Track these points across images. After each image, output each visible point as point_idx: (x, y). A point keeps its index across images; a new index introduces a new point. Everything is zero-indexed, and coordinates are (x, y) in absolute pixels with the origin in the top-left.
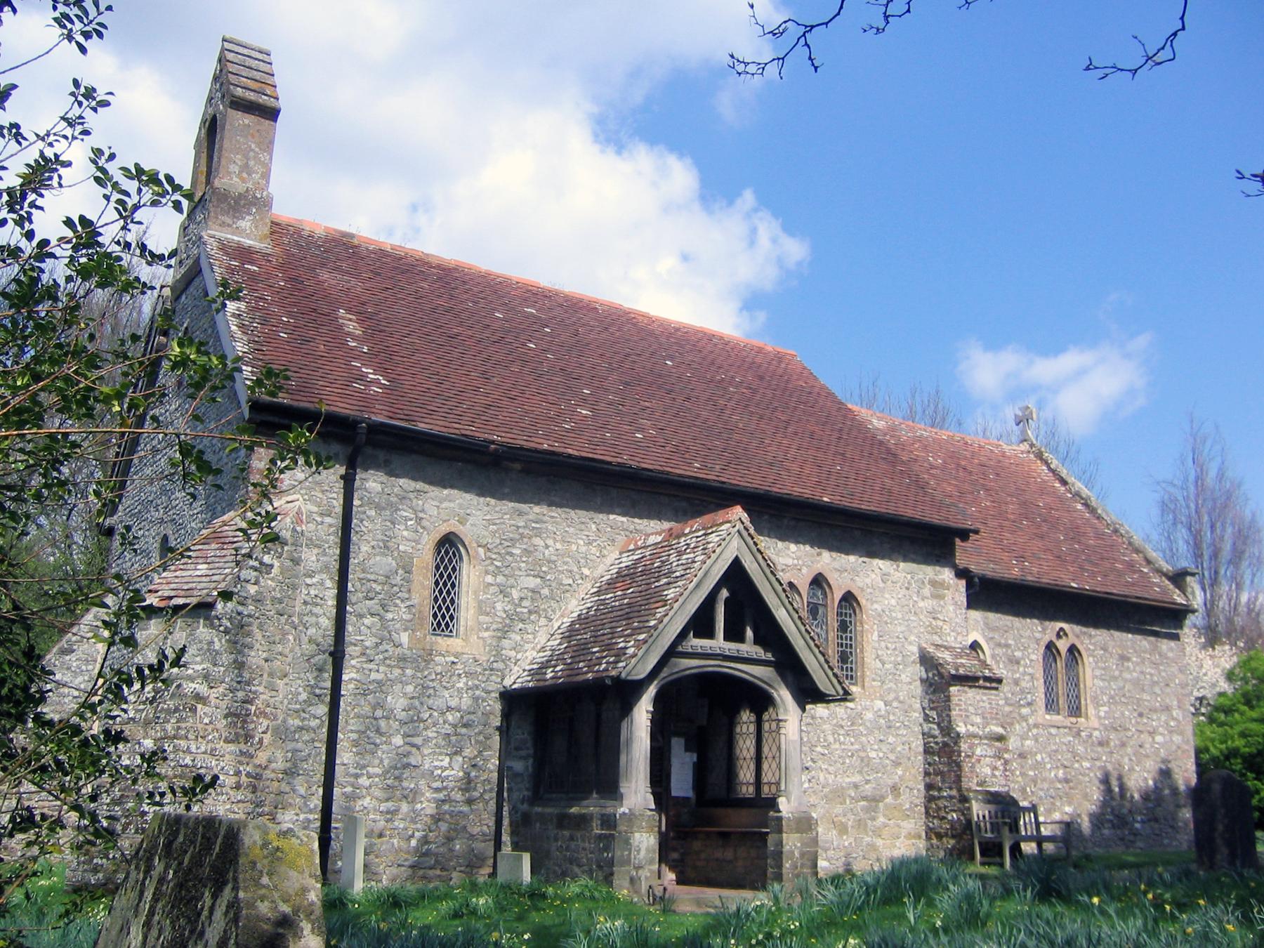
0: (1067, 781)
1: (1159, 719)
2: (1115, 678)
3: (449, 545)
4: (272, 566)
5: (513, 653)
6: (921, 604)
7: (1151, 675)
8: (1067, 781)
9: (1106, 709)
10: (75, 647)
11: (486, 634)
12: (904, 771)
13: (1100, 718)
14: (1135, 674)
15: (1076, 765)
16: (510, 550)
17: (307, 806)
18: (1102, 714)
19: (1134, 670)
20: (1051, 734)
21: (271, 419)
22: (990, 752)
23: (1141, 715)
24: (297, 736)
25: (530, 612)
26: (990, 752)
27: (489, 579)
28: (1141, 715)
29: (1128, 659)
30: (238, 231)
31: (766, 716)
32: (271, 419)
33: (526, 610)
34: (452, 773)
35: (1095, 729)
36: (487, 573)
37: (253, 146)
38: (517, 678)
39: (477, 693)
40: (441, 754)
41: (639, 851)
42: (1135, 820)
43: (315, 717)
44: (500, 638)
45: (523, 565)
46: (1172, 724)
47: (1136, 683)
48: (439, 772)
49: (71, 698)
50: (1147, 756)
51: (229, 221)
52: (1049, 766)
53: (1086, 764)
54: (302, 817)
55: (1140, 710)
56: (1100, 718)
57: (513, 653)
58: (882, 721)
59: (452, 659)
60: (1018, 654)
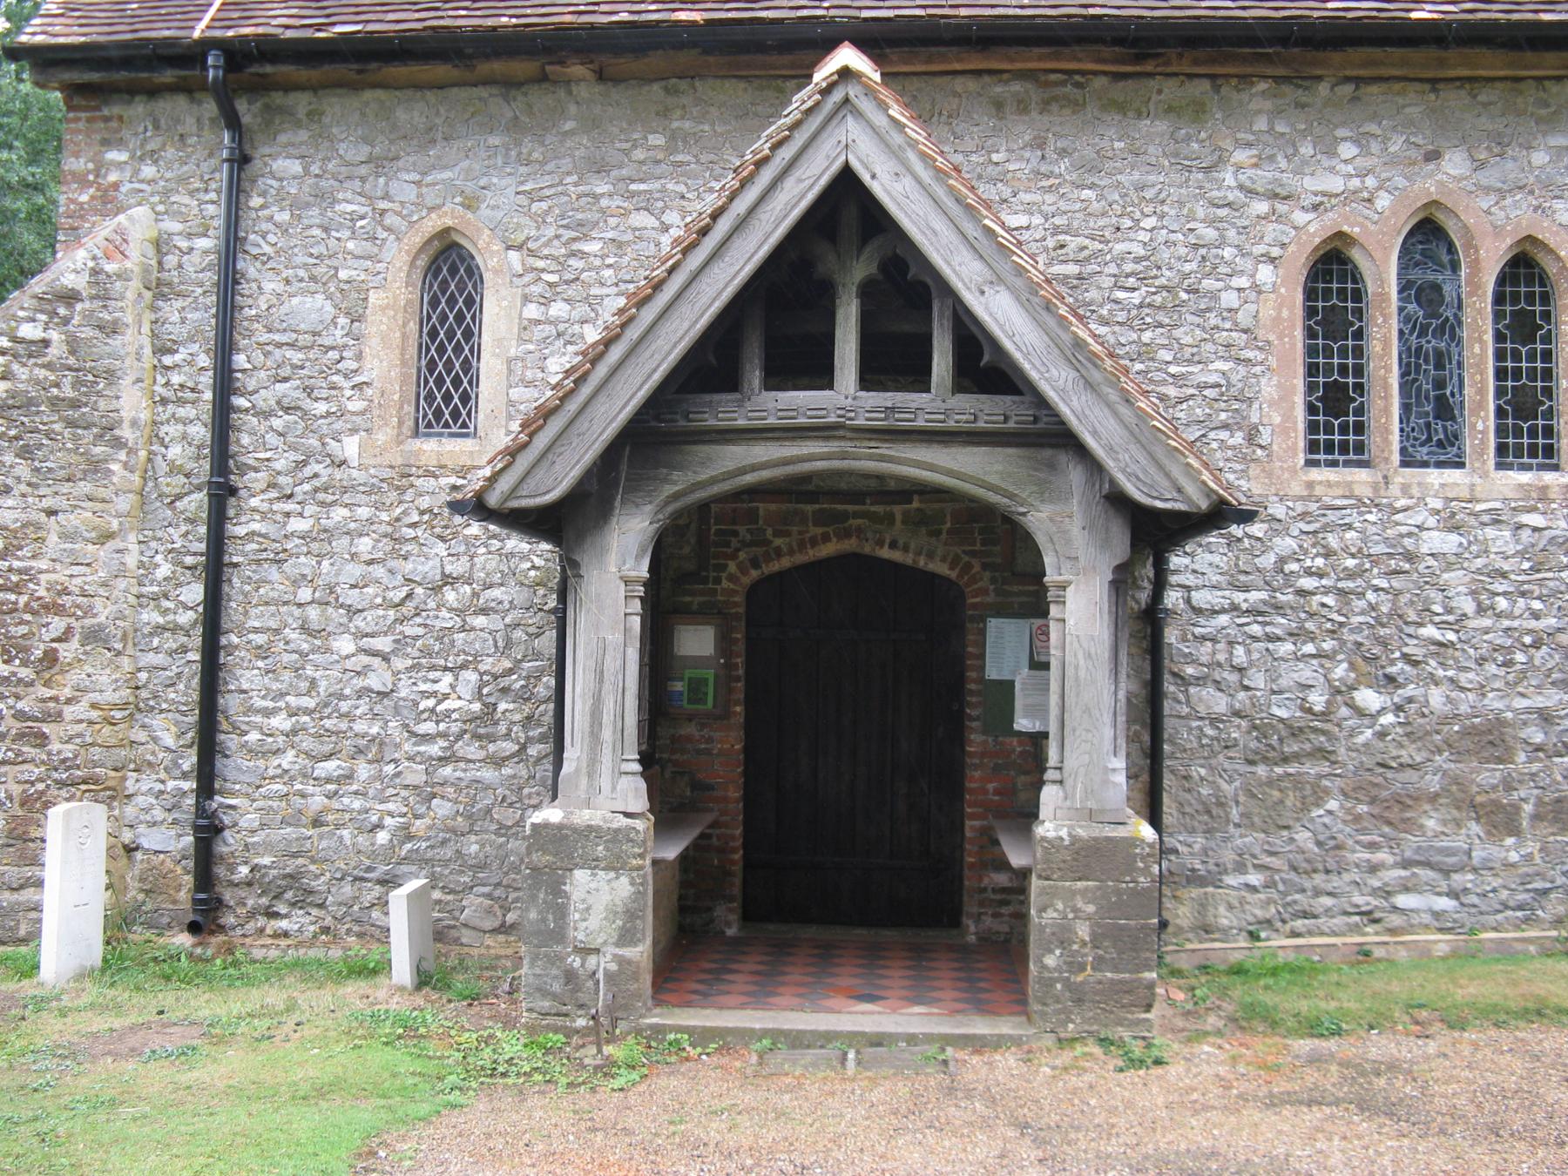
4: (46, 343)
21: (94, 77)
32: (94, 77)
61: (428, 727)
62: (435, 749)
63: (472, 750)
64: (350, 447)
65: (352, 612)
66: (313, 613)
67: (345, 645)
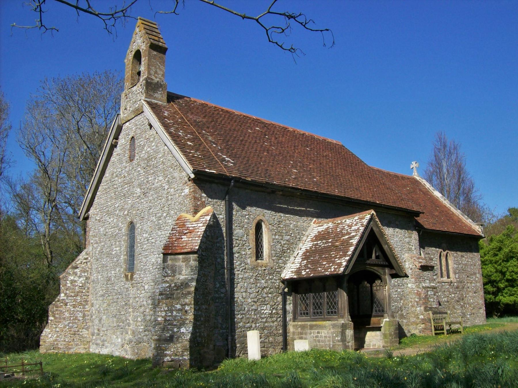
0: (448, 302)
1: (473, 278)
2: (460, 264)
3: (258, 227)
5: (283, 265)
6: (405, 240)
7: (470, 262)
8: (448, 302)
9: (458, 275)
10: (78, 266)
11: (275, 258)
12: (404, 301)
13: (456, 278)
14: (466, 262)
15: (450, 296)
16: (279, 225)
17: (222, 327)
18: (457, 277)
19: (465, 261)
20: (442, 285)
22: (432, 293)
23: (468, 277)
24: (217, 301)
25: (287, 249)
26: (432, 293)
27: (273, 237)
28: (468, 277)
29: (464, 257)
30: (155, 98)
31: (374, 285)
33: (286, 248)
34: (267, 311)
35: (455, 282)
36: (273, 234)
37: (158, 63)
38: (288, 274)
39: (273, 281)
40: (263, 304)
41: (348, 336)
42: (468, 315)
43: (222, 293)
44: (279, 260)
45: (284, 231)
46: (477, 279)
47: (466, 265)
48: (263, 311)
49: (78, 287)
50: (470, 291)
51: (152, 93)
52: (442, 297)
53: (453, 295)
54: (221, 331)
55: (468, 275)
56: (456, 278)
57: (283, 265)
58: (396, 284)
59: (264, 268)
60: (432, 256)
61: (263, 316)
62: (264, 320)
63: (270, 320)
64: (249, 261)
65: (250, 293)
66: (244, 294)
67: (250, 300)
